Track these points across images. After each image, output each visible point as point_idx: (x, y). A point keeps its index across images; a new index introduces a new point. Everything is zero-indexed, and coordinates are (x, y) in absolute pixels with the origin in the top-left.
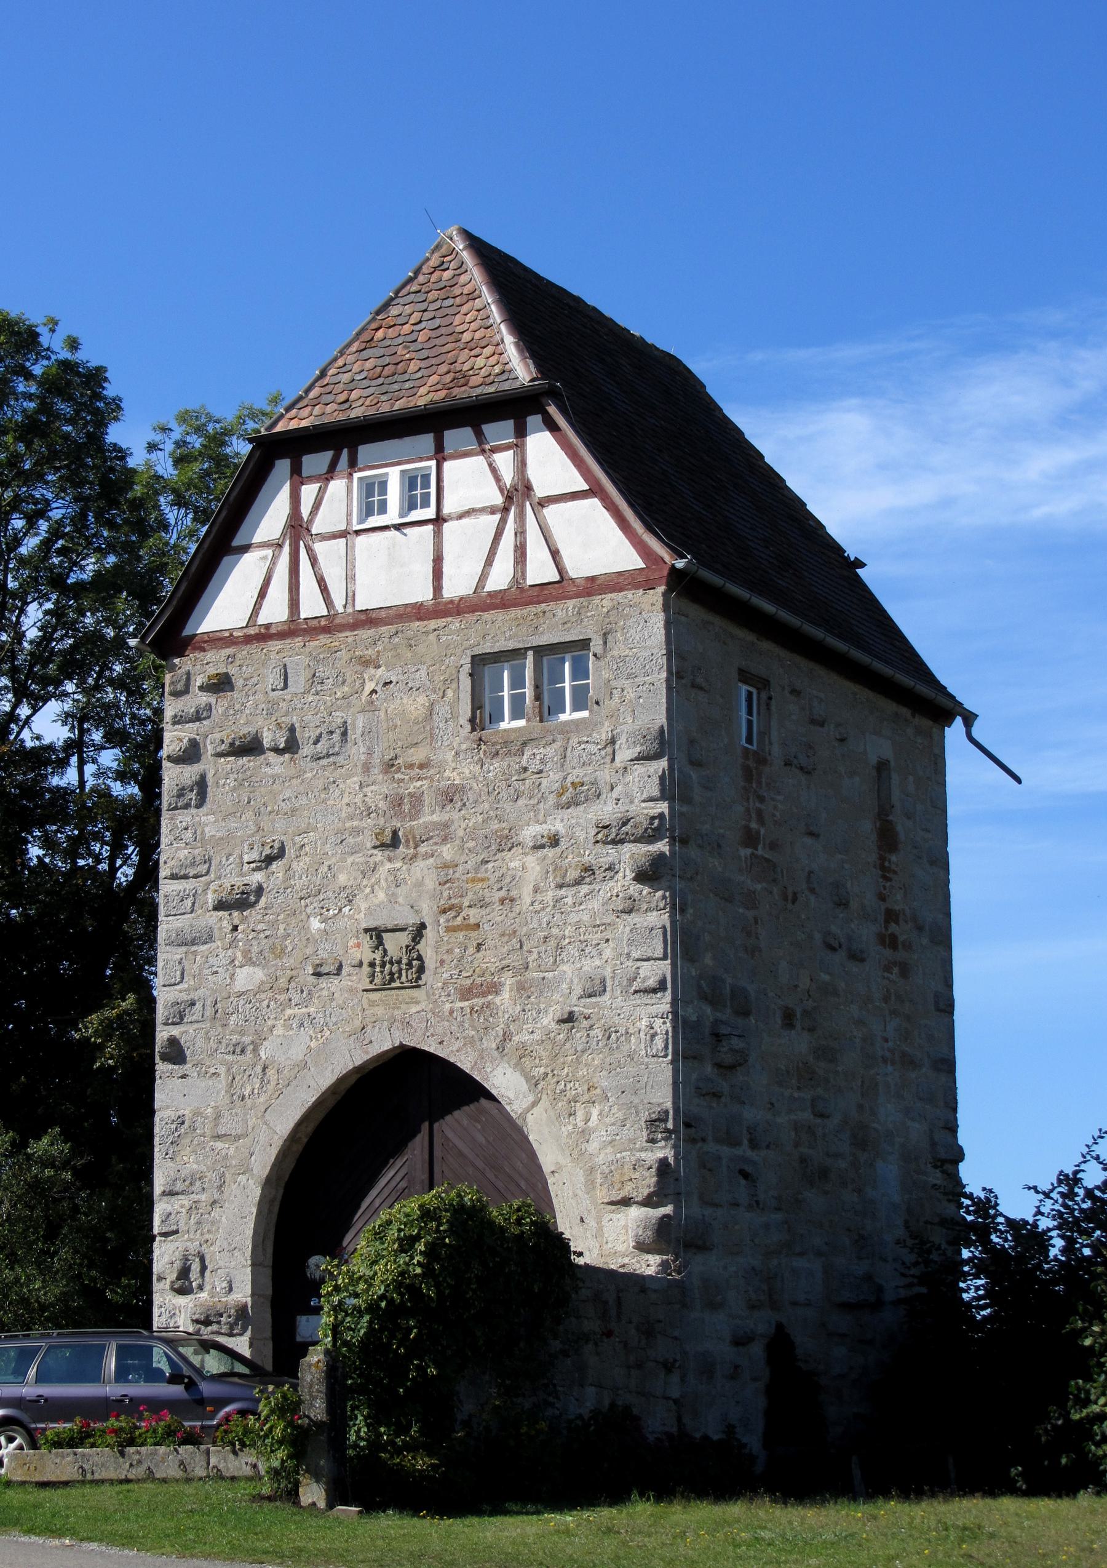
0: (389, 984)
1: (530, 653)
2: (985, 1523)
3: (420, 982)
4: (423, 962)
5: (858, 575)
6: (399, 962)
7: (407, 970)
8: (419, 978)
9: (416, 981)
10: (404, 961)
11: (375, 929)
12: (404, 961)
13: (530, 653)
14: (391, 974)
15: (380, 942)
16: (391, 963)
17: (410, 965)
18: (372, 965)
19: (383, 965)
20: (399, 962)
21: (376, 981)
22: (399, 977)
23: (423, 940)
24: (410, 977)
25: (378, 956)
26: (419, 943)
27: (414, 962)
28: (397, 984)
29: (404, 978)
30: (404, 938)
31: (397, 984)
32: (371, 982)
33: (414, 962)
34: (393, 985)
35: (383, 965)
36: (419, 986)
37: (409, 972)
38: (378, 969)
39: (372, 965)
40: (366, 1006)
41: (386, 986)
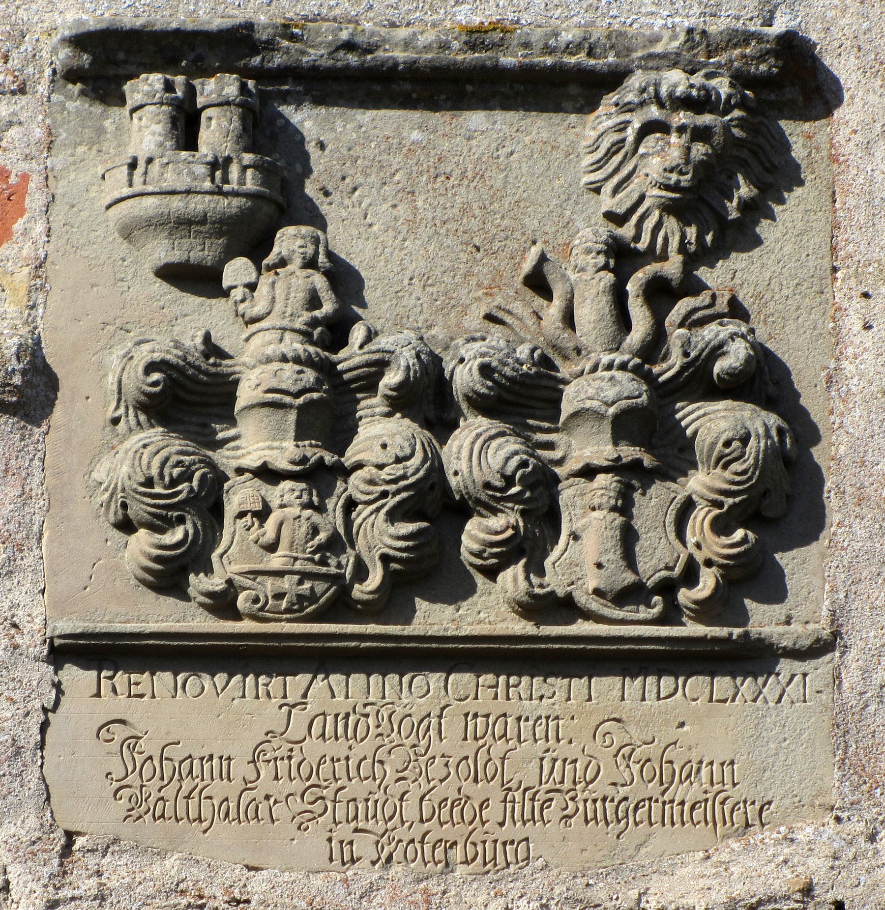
0: (395, 599)
1: (249, 515)
2: (106, 875)
3: (763, 620)
4: (801, 430)
5: (309, 673)
6: (525, 398)
7: (631, 477)
8: (753, 578)
9: (722, 606)
10: (596, 386)
11: (231, 46)
12: (596, 386)
13: (249, 515)
14: (435, 505)
15: (275, 203)
16: (429, 400)
17: (653, 439)
18: (190, 397)
19: (328, 414)
20: (525, 398)
21: (235, 554)
22: (534, 539)
23: (794, 211)
24: (657, 555)
25: (259, 334)
26: (738, 235)
27: (711, 422)
28: (491, 610)
29: (582, 557)
30: (566, 184)
31: (491, 610)
32: (168, 577)
33: (711, 422)
34: (432, 618)
35: (328, 414)
36: (752, 658)
37: (654, 504)
38: (258, 440)
39: (190, 397)
40: (93, 813)
41: (343, 631)
